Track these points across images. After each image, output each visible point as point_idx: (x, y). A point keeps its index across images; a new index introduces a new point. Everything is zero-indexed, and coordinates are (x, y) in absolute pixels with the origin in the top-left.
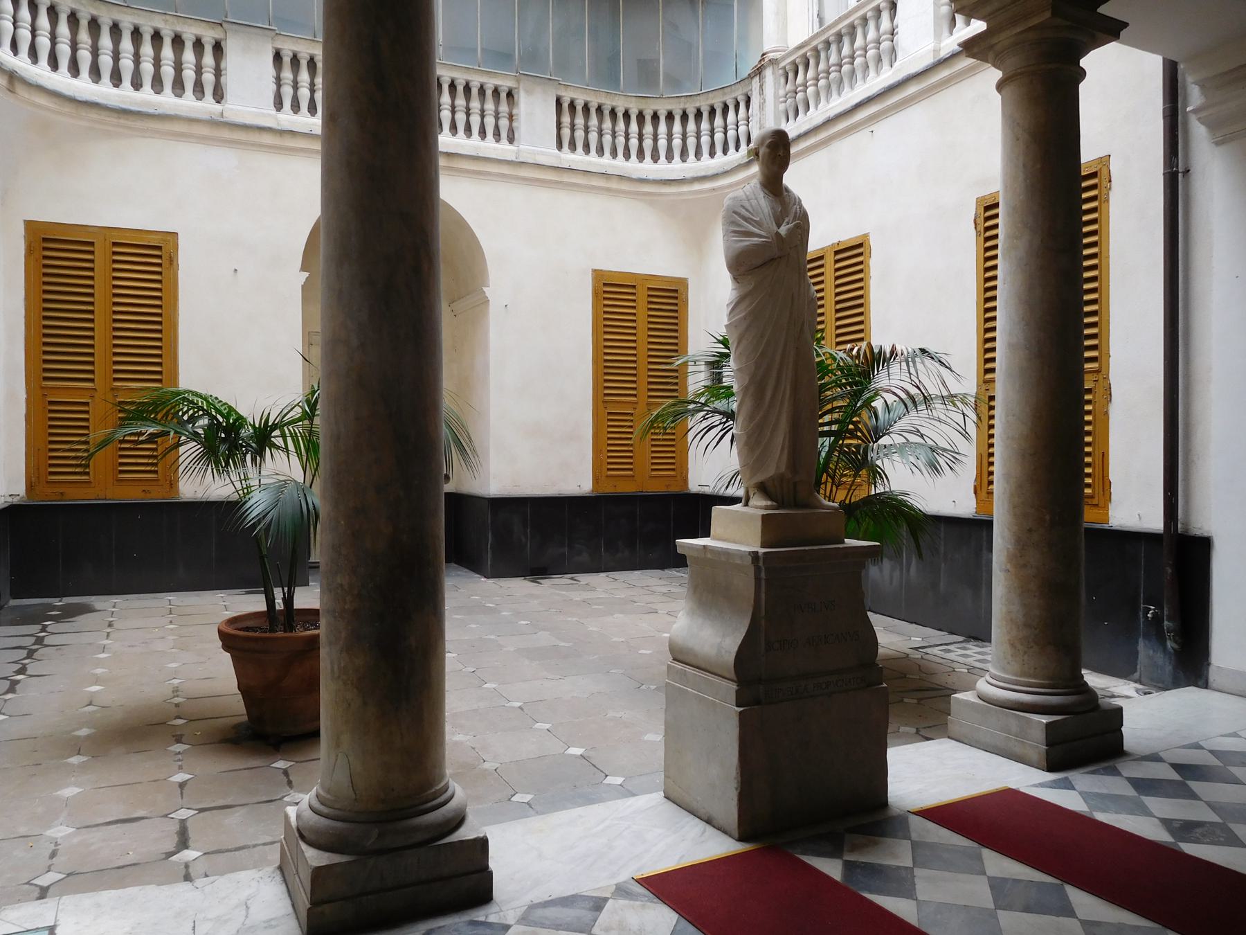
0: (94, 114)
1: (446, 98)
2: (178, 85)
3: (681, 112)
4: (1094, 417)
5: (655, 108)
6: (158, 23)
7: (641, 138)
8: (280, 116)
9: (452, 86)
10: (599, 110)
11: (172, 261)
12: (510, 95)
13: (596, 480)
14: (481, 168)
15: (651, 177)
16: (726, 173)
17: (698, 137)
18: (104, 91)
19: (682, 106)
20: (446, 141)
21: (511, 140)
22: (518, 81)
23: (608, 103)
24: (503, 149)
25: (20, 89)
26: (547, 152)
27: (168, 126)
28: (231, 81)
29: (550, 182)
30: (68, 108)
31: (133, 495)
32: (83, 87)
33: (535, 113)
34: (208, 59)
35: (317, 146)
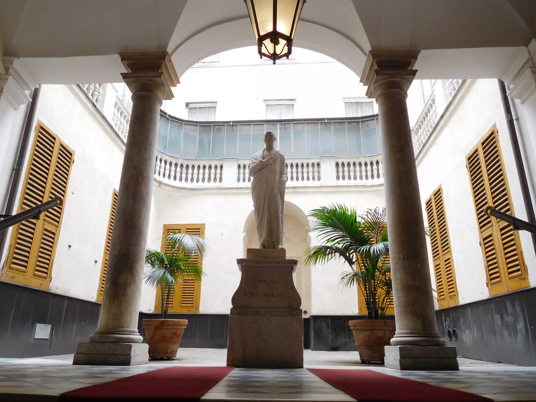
0: (183, 191)
1: (289, 169)
4: (13, 255)
5: (377, 159)
6: (355, 160)
7: (343, 172)
8: (338, 182)
9: (292, 166)
10: (354, 164)
12: (318, 165)
18: (189, 185)
21: (319, 179)
24: (316, 183)
25: (162, 186)
26: (335, 182)
27: (207, 191)
28: (322, 174)
29: (334, 192)
30: (176, 190)
32: (183, 184)
33: (328, 170)
34: (218, 170)
35: (250, 191)
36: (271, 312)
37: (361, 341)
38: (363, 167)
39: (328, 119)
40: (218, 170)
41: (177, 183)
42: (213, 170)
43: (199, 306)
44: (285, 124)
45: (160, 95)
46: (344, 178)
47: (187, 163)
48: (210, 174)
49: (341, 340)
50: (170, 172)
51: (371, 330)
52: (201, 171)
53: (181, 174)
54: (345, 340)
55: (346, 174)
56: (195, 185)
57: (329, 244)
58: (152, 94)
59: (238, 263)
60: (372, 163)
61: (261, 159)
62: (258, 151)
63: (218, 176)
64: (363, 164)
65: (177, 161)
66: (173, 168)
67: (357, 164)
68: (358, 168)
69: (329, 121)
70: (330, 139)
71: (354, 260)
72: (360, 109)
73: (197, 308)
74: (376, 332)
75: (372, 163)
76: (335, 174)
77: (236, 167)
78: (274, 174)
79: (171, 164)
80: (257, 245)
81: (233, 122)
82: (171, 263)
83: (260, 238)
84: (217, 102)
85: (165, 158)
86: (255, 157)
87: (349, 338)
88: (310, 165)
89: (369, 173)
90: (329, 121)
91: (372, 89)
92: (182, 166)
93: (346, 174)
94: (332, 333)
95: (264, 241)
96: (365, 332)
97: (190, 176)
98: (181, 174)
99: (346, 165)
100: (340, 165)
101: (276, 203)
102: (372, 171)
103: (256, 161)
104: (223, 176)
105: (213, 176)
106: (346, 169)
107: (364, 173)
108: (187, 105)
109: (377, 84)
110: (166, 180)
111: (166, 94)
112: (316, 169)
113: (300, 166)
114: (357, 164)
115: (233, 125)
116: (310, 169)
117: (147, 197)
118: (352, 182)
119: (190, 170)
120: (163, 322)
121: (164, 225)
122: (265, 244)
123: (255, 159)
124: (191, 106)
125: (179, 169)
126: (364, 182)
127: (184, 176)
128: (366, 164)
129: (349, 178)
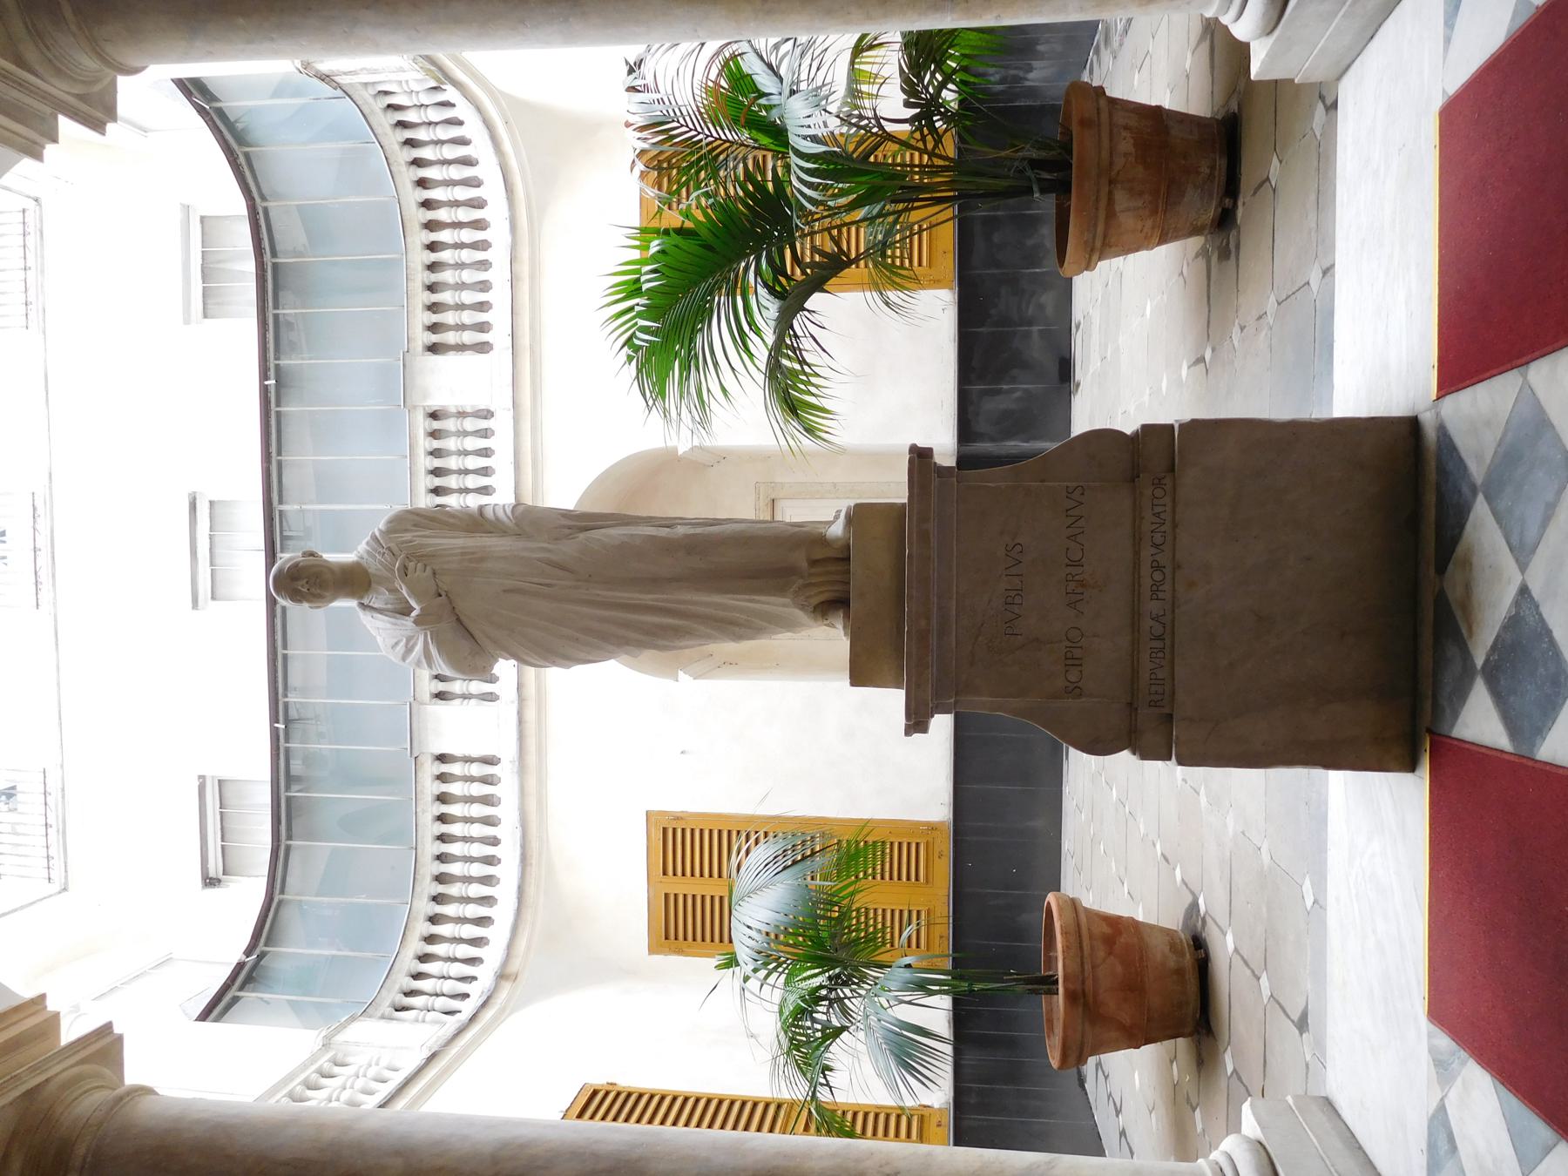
0: (531, 890)
1: (453, 501)
2: (482, 307)
3: (413, 168)
7: (461, 327)
11: (678, 817)
12: (434, 416)
13: (936, 283)
14: (528, 417)
15: (507, 214)
16: (479, 109)
17: (439, 142)
18: (507, 872)
19: (404, 168)
20: (502, 498)
21: (487, 414)
22: (415, 407)
23: (422, 277)
24: (502, 424)
30: (528, 916)
31: (944, 870)
32: (505, 893)
33: (451, 381)
34: (455, 769)
35: (530, 672)
36: (1157, 567)
37: (1149, 223)
38: (445, 256)
39: (264, 375)
40: (455, 769)
41: (503, 914)
42: (455, 788)
43: (927, 824)
44: (283, 538)
45: (90, 1103)
46: (483, 327)
47: (428, 879)
48: (470, 800)
49: (1036, 349)
50: (460, 940)
51: (1111, 182)
52: (456, 829)
53: (467, 900)
54: (1035, 336)
55: (468, 317)
56: (508, 853)
57: (762, 354)
58: (81, 1150)
59: (924, 730)
60: (431, 226)
61: (408, 622)
62: (372, 640)
63: (476, 770)
64: (434, 257)
65: (422, 917)
66: (444, 930)
67: (434, 277)
68: (447, 276)
69: (272, 373)
70: (339, 372)
71: (830, 247)
72: (229, 266)
73: (932, 827)
74: (1119, 162)
75: (431, 226)
76: (469, 358)
77: (441, 708)
78: (482, 560)
79: (430, 939)
80: (833, 640)
81: (274, 718)
82: (823, 962)
83: (789, 625)
84: (202, 778)
85: (408, 963)
86: (401, 648)
87: (1030, 323)
88: (436, 444)
89: (467, 235)
90: (272, 373)
91: (59, 88)
92: (437, 899)
93: (468, 317)
94: (1014, 380)
95: (802, 608)
96: (1117, 208)
97: (477, 870)
98: (467, 900)
99: (435, 318)
100: (434, 338)
101: (626, 550)
102: (458, 225)
103: (419, 647)
104: (475, 754)
105: (477, 789)
106: (449, 318)
107: (466, 255)
108: (210, 882)
109: (31, 54)
110: (492, 956)
111: (86, 1068)
112: (450, 425)
113: (438, 482)
114: (434, 277)
115: (287, 722)
116: (451, 444)
117: (595, 1156)
118: (499, 296)
119: (455, 869)
120: (1071, 997)
121: (653, 950)
122: (815, 601)
123: (409, 650)
124: (215, 868)
125: (450, 910)
126: (498, 255)
127: (476, 890)
128: (432, 247)
129: (482, 307)
